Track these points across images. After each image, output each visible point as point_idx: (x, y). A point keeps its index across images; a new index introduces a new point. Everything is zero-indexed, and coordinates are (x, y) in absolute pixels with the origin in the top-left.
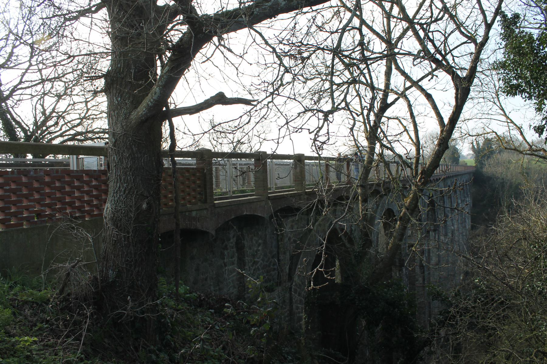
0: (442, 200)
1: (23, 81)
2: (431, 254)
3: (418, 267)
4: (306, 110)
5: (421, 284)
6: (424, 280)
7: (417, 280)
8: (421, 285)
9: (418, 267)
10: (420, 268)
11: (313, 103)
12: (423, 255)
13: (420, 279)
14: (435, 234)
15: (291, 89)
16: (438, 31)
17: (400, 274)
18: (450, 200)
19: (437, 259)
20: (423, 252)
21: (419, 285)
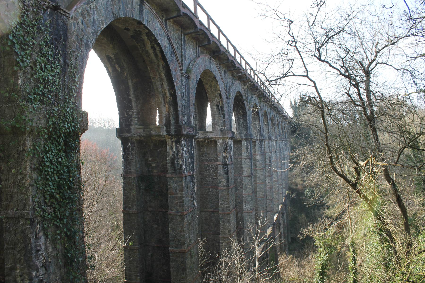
0: (257, 119)
1: (293, 74)
2: (243, 166)
3: (220, 166)
4: (416, 78)
5: (224, 186)
6: (228, 181)
7: (220, 182)
8: (225, 188)
9: (220, 166)
10: (223, 167)
11: (343, 19)
12: (226, 151)
13: (224, 181)
14: (247, 144)
15: (265, 40)
16: (290, 29)
17: (177, 148)
18: (267, 127)
19: (250, 170)
20: (227, 147)
21: (222, 188)
